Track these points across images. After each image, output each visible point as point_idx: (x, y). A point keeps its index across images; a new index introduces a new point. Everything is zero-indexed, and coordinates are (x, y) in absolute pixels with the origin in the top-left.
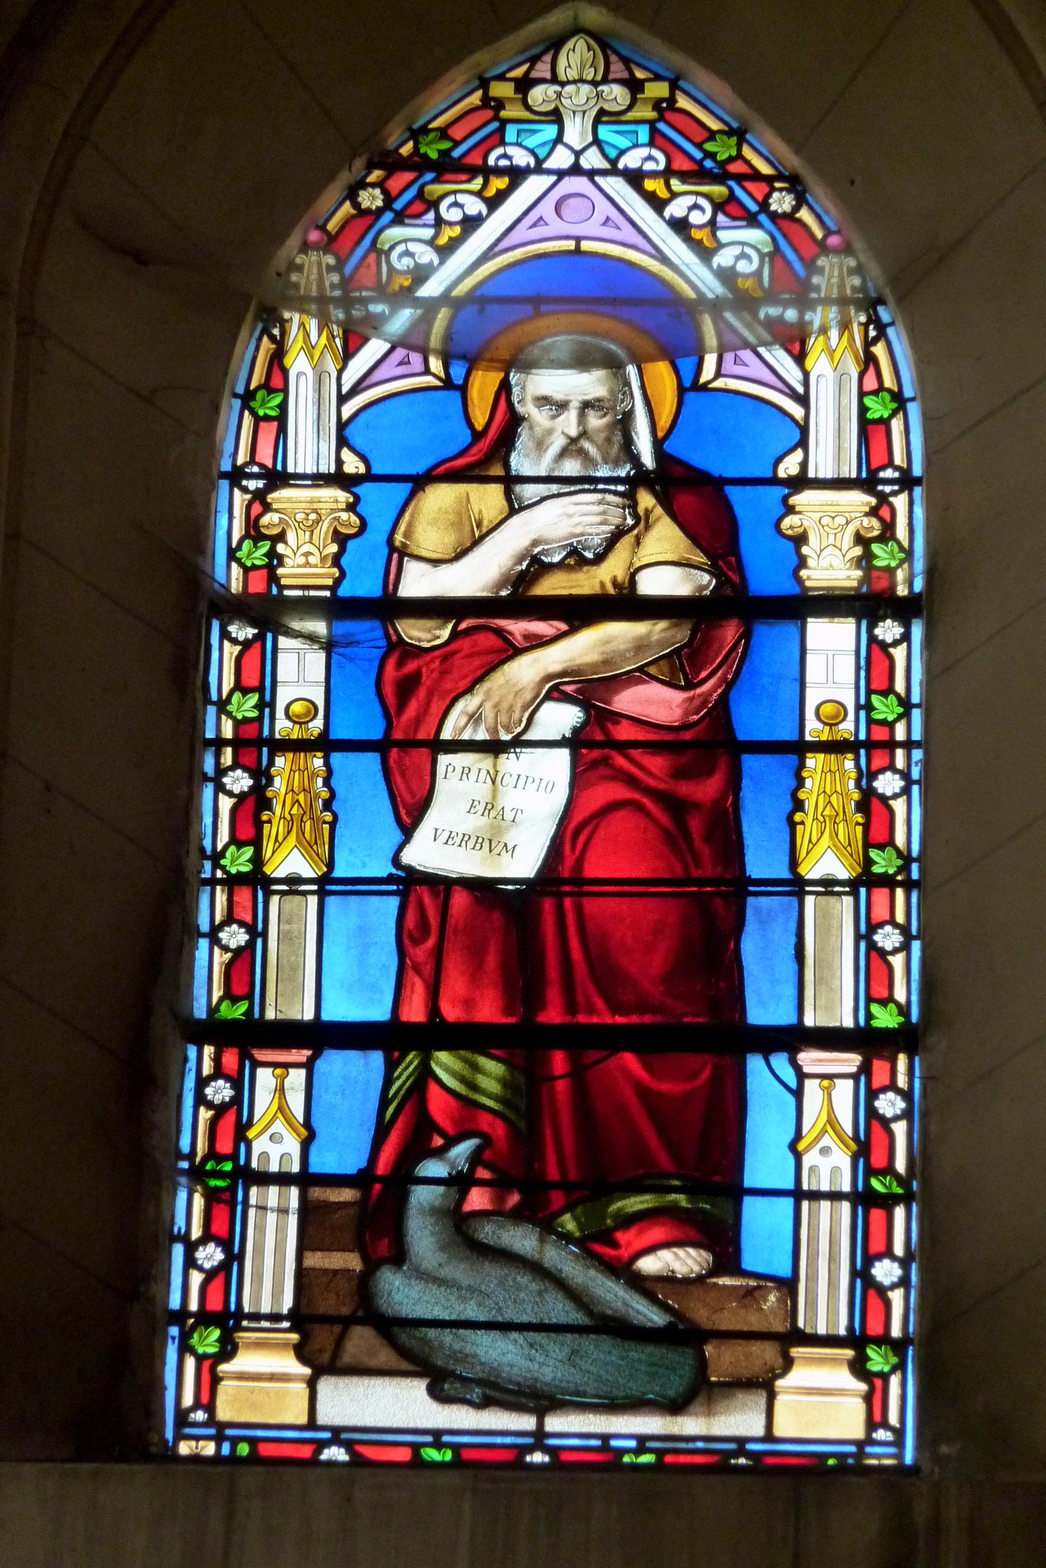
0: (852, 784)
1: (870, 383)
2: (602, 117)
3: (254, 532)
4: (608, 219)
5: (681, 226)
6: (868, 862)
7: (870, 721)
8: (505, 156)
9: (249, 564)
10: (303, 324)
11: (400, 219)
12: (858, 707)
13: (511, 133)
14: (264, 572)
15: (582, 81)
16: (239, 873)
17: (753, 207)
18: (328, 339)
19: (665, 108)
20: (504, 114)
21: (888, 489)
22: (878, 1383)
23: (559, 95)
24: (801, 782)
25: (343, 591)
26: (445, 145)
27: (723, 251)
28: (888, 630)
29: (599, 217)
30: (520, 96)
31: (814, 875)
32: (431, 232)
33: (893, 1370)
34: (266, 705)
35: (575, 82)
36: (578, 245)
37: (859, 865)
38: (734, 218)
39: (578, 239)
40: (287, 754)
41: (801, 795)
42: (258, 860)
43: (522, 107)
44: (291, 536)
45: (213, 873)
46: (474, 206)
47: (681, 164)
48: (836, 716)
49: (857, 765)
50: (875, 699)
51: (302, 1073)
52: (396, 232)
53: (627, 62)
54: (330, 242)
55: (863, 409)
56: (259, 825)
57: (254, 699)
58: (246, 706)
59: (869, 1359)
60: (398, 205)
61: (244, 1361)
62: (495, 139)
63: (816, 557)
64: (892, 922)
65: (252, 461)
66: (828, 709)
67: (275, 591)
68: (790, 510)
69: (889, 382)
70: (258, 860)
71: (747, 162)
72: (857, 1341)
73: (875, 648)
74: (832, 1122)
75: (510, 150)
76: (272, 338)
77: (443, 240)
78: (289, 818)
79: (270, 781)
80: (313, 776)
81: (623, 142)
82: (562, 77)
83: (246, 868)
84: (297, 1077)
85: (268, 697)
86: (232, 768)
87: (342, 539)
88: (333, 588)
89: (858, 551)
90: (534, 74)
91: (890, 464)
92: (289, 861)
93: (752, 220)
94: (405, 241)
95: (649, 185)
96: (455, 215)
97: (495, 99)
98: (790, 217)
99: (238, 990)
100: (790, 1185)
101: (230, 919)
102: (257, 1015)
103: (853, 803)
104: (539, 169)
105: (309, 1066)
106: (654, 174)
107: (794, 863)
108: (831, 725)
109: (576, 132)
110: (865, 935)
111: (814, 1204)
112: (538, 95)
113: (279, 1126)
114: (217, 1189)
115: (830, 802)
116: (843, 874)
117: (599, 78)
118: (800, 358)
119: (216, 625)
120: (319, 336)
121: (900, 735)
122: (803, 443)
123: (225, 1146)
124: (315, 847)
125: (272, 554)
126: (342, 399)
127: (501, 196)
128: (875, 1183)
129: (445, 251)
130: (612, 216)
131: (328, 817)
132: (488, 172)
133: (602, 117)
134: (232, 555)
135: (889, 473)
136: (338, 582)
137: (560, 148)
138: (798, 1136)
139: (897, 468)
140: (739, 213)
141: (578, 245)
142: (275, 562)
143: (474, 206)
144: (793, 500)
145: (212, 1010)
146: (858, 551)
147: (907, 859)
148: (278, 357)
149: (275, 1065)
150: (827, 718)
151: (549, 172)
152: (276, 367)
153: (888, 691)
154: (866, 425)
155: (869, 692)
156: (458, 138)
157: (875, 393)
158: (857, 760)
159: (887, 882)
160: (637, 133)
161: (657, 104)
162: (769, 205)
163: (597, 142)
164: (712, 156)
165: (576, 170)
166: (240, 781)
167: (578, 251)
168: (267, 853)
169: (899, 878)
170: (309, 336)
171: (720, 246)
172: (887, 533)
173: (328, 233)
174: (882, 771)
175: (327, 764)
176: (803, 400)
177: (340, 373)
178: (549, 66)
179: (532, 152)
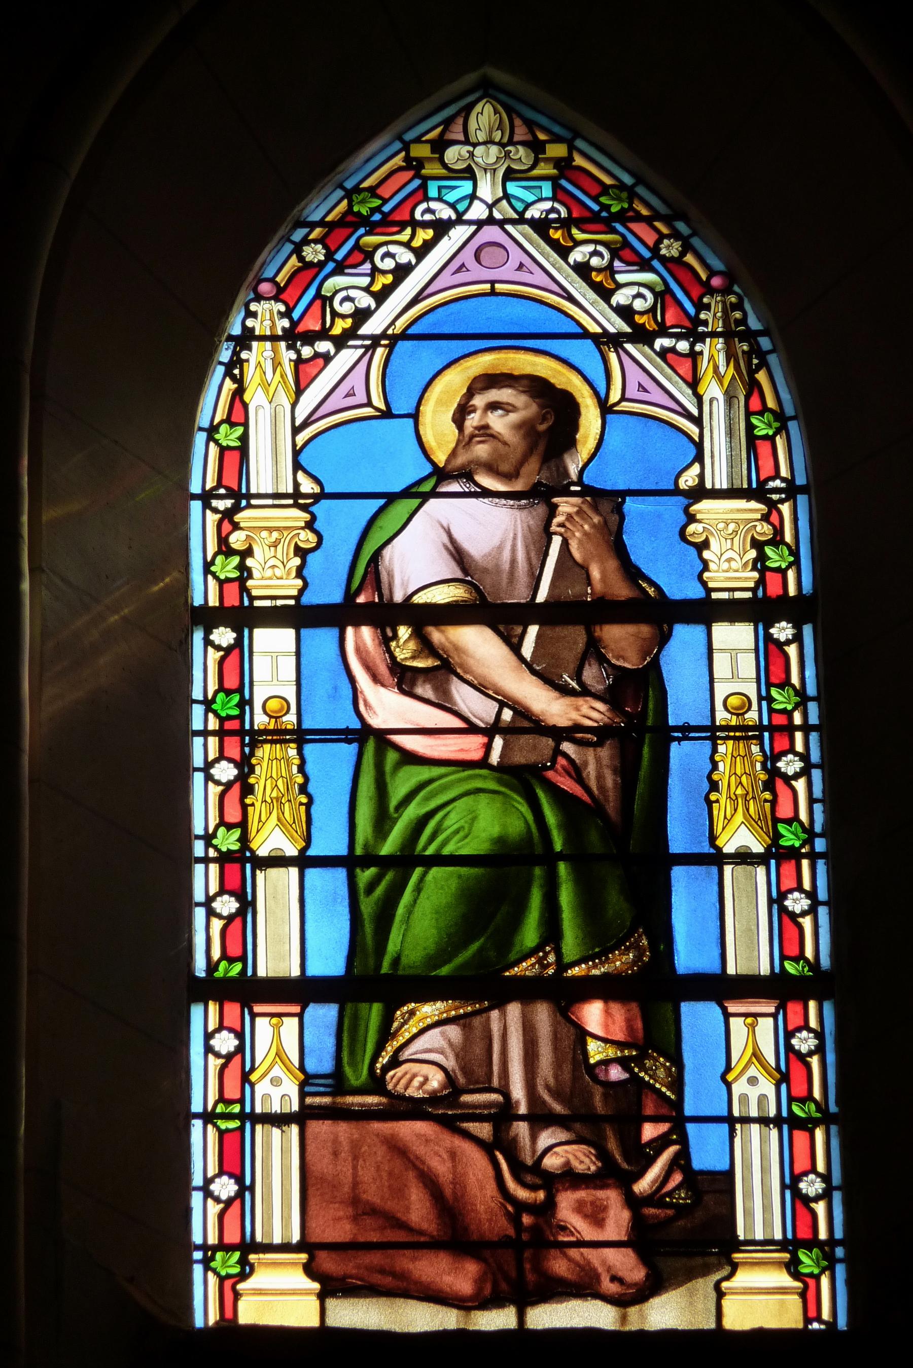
0: (758, 766)
1: (755, 404)
2: (510, 175)
3: (225, 549)
5: (583, 270)
6: (777, 836)
7: (771, 711)
8: (429, 210)
9: (223, 714)
11: (340, 270)
12: (760, 698)
14: (236, 585)
15: (491, 142)
17: (647, 254)
19: (564, 166)
20: (423, 171)
21: (775, 497)
22: (811, 1282)
24: (715, 766)
25: (306, 600)
28: (782, 631)
29: (513, 263)
30: (437, 156)
31: (729, 849)
33: (823, 1272)
34: (245, 703)
36: (493, 288)
37: (769, 837)
38: (628, 264)
39: (493, 283)
41: (715, 777)
42: (244, 840)
43: (438, 165)
44: (257, 549)
45: (206, 852)
46: (405, 256)
49: (762, 750)
50: (774, 692)
51: (296, 1020)
53: (530, 125)
55: (750, 427)
56: (244, 808)
58: (228, 706)
59: (801, 1262)
60: (339, 256)
61: (259, 1279)
63: (717, 561)
64: (800, 888)
65: (219, 484)
66: (734, 701)
67: (246, 603)
69: (771, 403)
70: (244, 840)
72: (791, 1246)
73: (772, 647)
74: (757, 1055)
75: (433, 205)
76: (234, 379)
77: (377, 287)
78: (269, 801)
79: (252, 770)
81: (529, 197)
82: (473, 139)
83: (236, 847)
84: (291, 1024)
87: (302, 553)
88: (297, 598)
89: (753, 554)
91: (777, 475)
92: (270, 839)
93: (644, 266)
94: (347, 288)
95: (557, 235)
96: (389, 264)
97: (416, 159)
100: (725, 1113)
101: (221, 757)
102: (250, 973)
105: (300, 1016)
107: (713, 838)
108: (738, 715)
109: (487, 189)
110: (777, 901)
111: (746, 1126)
112: (452, 154)
113: (277, 1071)
114: (228, 1130)
115: (741, 783)
116: (758, 848)
117: (505, 140)
118: (694, 383)
119: (198, 637)
121: (797, 719)
123: (232, 1092)
125: (242, 567)
126: (296, 431)
127: (428, 246)
128: (796, 1109)
129: (381, 297)
131: (767, 795)
132: (416, 225)
134: (207, 567)
135: (777, 483)
136: (301, 591)
137: (476, 202)
138: (728, 1068)
139: (784, 480)
140: (634, 258)
141: (493, 288)
142: (245, 575)
143: (405, 256)
144: (694, 508)
145: (212, 967)
147: (810, 834)
150: (272, 711)
151: (470, 223)
152: (237, 400)
153: (785, 683)
154: (752, 439)
155: (769, 685)
156: (387, 196)
157: (761, 413)
159: (793, 854)
160: (541, 187)
161: (558, 163)
163: (506, 196)
164: (606, 208)
165: (490, 220)
169: (803, 851)
170: (265, 373)
172: (777, 540)
173: (277, 284)
174: (784, 753)
176: (698, 421)
177: (294, 406)
178: (461, 128)
179: (453, 206)
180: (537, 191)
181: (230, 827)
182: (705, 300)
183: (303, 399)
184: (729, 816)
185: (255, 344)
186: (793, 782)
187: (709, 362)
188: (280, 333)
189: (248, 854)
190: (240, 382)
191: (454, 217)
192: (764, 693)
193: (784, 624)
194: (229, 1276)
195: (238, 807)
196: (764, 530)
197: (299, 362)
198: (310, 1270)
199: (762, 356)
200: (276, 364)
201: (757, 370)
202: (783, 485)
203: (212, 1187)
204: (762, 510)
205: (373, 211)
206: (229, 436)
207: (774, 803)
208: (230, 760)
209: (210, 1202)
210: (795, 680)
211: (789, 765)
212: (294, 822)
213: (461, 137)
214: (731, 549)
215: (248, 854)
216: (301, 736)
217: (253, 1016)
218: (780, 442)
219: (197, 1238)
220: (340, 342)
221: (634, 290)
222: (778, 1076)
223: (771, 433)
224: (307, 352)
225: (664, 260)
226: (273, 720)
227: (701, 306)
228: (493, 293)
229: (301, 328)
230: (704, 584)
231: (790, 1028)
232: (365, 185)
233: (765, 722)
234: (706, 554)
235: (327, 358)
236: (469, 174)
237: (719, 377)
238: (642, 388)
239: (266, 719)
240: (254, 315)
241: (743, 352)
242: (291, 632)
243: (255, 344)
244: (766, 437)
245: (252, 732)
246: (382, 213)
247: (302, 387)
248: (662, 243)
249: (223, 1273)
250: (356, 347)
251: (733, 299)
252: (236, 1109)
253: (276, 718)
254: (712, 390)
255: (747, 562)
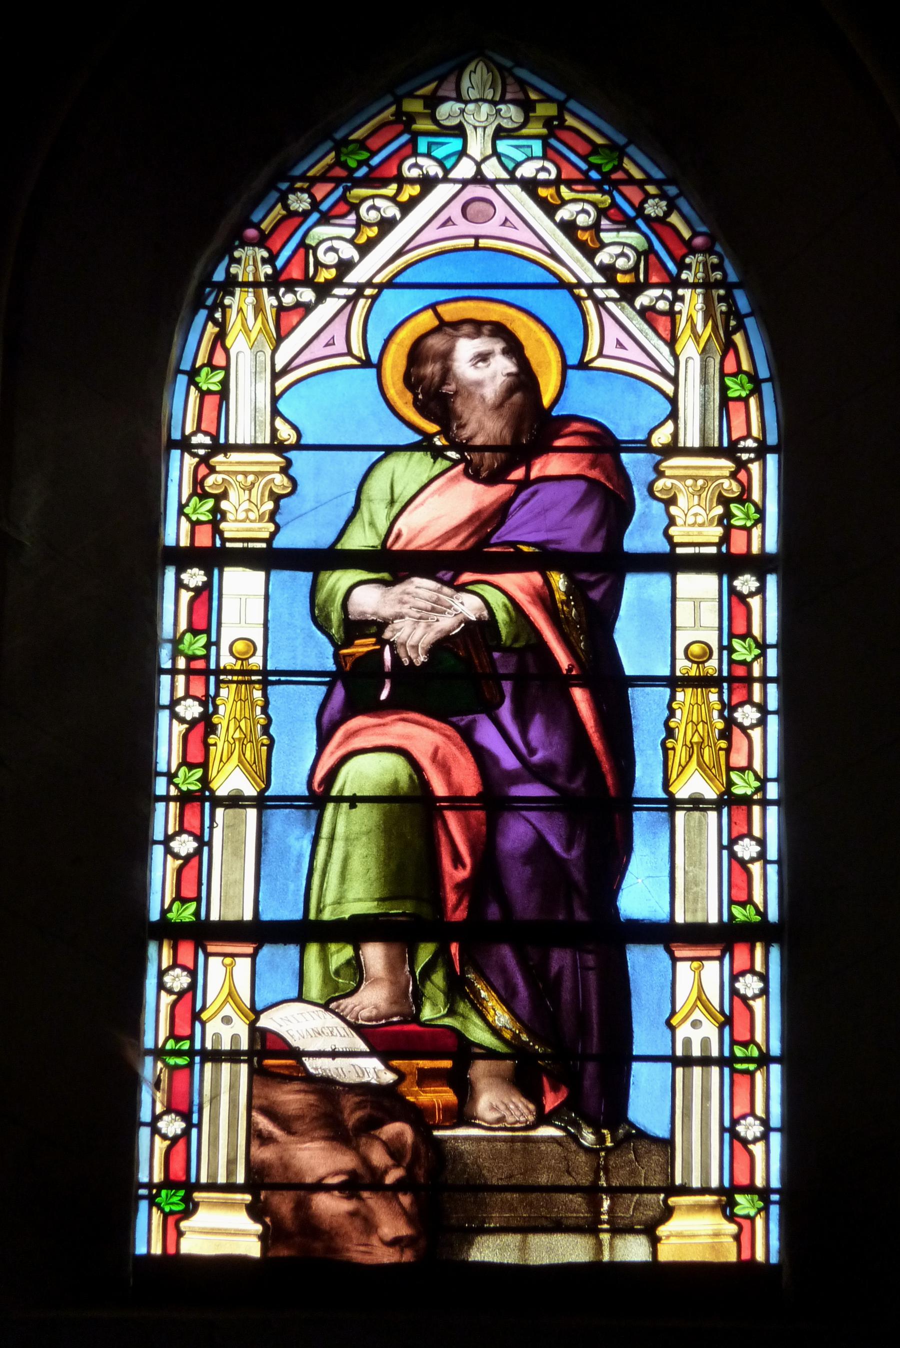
0: (715, 714)
1: (730, 366)
2: (500, 133)
3: (200, 492)
4: (506, 220)
5: (569, 228)
6: (730, 783)
7: (731, 662)
10: (241, 309)
11: (326, 219)
12: (721, 648)
13: (423, 145)
16: (189, 791)
17: (631, 213)
18: (263, 323)
20: (414, 127)
21: (745, 456)
22: (746, 1224)
23: (462, 111)
24: (672, 713)
25: (278, 543)
26: (365, 155)
27: (607, 250)
28: (746, 583)
31: (222, 792)
32: (352, 231)
35: (476, 101)
36: (477, 243)
38: (614, 222)
39: (477, 238)
40: (686, 690)
41: (672, 724)
42: (205, 780)
44: (232, 493)
45: (168, 790)
46: (391, 211)
47: (569, 173)
48: (246, 653)
50: (736, 643)
51: (248, 961)
52: (322, 231)
53: (523, 85)
54: (262, 241)
55: (724, 388)
56: (207, 746)
57: (203, 639)
60: (324, 207)
61: (203, 1218)
62: (408, 150)
66: (696, 649)
67: (218, 543)
68: (660, 474)
69: (745, 366)
71: (626, 172)
76: (216, 323)
77: (362, 240)
80: (253, 704)
81: (519, 156)
82: (465, 96)
85: (214, 639)
86: (184, 698)
87: (277, 498)
88: (269, 541)
89: (720, 510)
90: (441, 93)
91: (749, 435)
93: (630, 225)
95: (543, 192)
98: (662, 220)
99: (188, 891)
103: (717, 731)
104: (446, 180)
105: (253, 956)
106: (546, 184)
108: (698, 663)
110: (728, 847)
113: (228, 1010)
114: (177, 1067)
115: (697, 730)
116: (710, 793)
117: (497, 98)
118: (672, 342)
120: (256, 319)
122: (673, 415)
124: (254, 766)
125: (216, 510)
126: (276, 376)
129: (364, 249)
130: (509, 218)
131: (723, 744)
132: (401, 181)
133: (500, 133)
135: (750, 443)
136: (273, 535)
137: (465, 160)
138: (673, 1013)
140: (620, 218)
141: (477, 243)
142: (219, 516)
145: (164, 912)
146: (720, 510)
147: (764, 781)
148: (220, 338)
149: (225, 955)
150: (239, 653)
151: (455, 181)
154: (725, 401)
155: (731, 636)
158: (721, 693)
159: (746, 801)
160: (531, 147)
162: (644, 209)
163: (495, 153)
164: (598, 168)
165: (479, 179)
166: (191, 710)
167: (476, 248)
168: (213, 772)
169: (755, 797)
171: (603, 245)
172: (744, 498)
174: (742, 704)
175: (265, 695)
176: (674, 380)
177: (274, 352)
178: (453, 86)
179: (440, 163)
180: (528, 151)
181: (191, 766)
182: (688, 260)
183: (284, 345)
184: (683, 763)
185: (238, 290)
186: (749, 731)
187: (687, 321)
188: (263, 280)
189: (207, 793)
190: (222, 327)
191: (441, 175)
192: (725, 643)
193: (747, 577)
194: (172, 1213)
195: (200, 747)
196: (732, 488)
197: (281, 309)
198: (255, 1211)
199: (740, 318)
200: (258, 309)
201: (735, 332)
202: (755, 445)
203: (160, 1124)
204: (729, 467)
205: (361, 164)
206: (210, 381)
207: (728, 751)
208: (195, 698)
209: (157, 1138)
210: (756, 631)
211: (747, 715)
212: (255, 763)
213: (454, 95)
214: (699, 505)
215: (207, 793)
216: (267, 678)
217: (207, 955)
218: (753, 401)
219: (143, 1177)
220: (323, 291)
221: (617, 250)
222: (722, 1019)
223: (744, 394)
224: (288, 299)
225: (648, 219)
226: (240, 662)
227: (682, 266)
228: (476, 248)
229: (284, 277)
230: (669, 538)
231: (736, 971)
232: (354, 136)
233: (725, 674)
234: (673, 510)
235: (306, 309)
236: (459, 131)
237: (696, 337)
238: (620, 345)
239: (233, 660)
240: (238, 261)
241: (722, 312)
242: (262, 574)
243: (238, 290)
244: (739, 399)
245: (218, 672)
246: (369, 166)
247: (283, 334)
248: (647, 202)
249: (167, 1209)
250: (339, 297)
251: (715, 260)
252: (186, 1045)
253: (242, 660)
254: (689, 349)
255: (713, 518)
